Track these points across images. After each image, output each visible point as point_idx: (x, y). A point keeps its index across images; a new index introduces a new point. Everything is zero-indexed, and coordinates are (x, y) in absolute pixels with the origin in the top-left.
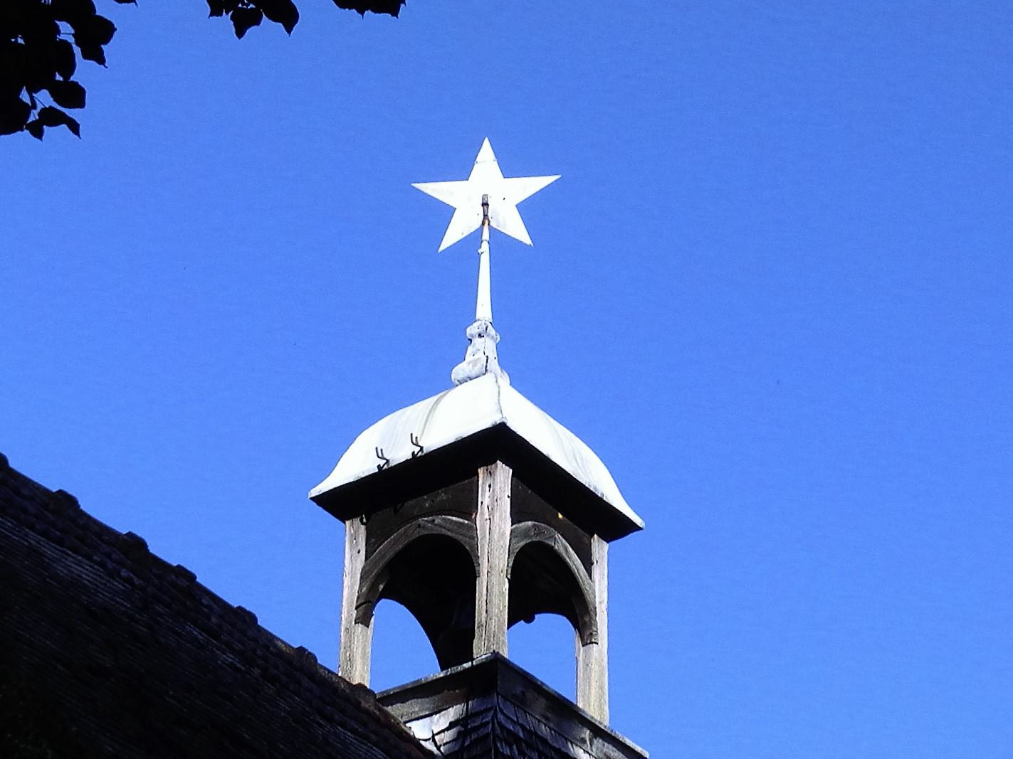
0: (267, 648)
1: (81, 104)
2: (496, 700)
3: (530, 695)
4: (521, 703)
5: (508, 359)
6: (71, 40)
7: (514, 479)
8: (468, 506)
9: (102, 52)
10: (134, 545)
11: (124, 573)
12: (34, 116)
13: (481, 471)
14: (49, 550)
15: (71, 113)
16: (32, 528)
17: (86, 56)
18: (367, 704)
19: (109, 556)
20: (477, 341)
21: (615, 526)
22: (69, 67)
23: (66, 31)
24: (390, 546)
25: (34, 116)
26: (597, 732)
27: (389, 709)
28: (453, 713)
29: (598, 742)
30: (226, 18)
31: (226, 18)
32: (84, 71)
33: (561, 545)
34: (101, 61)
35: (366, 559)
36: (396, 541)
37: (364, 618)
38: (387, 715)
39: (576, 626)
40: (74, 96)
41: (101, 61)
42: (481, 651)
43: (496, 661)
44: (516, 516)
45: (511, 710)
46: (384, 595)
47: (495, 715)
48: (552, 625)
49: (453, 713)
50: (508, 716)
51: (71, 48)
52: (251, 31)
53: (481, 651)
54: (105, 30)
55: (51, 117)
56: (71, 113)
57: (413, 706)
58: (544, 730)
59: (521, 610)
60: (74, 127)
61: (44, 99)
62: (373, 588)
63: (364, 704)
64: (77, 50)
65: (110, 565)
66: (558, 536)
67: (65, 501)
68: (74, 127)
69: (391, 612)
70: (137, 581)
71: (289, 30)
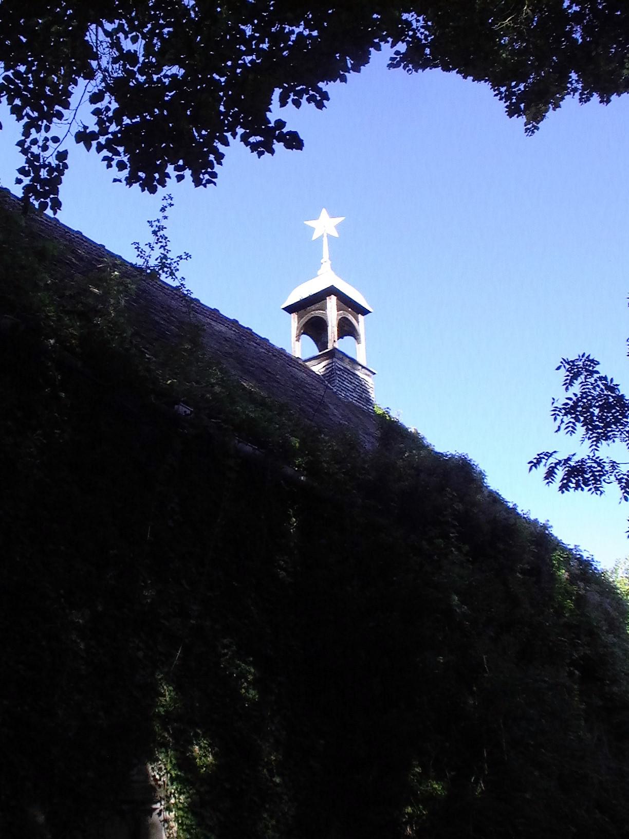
0: (273, 348)
1: (216, 178)
2: (335, 359)
3: (344, 358)
4: (342, 360)
5: (333, 268)
6: (213, 159)
7: (326, 340)
8: (324, 308)
9: (221, 162)
10: (235, 322)
11: (234, 329)
12: (204, 182)
13: (327, 298)
14: (213, 323)
15: (213, 180)
16: (208, 318)
17: (218, 164)
18: (300, 362)
19: (229, 324)
20: (324, 263)
21: (365, 312)
22: (212, 168)
23: (212, 157)
24: (305, 319)
25: (204, 182)
26: (363, 367)
27: (306, 363)
28: (324, 363)
29: (363, 369)
30: (255, 153)
31: (255, 153)
32: (217, 168)
33: (350, 317)
34: (221, 165)
35: (298, 323)
36: (306, 319)
37: (298, 339)
38: (306, 365)
39: (356, 339)
40: (214, 175)
41: (221, 165)
42: (330, 347)
43: (335, 350)
44: (338, 310)
45: (339, 362)
46: (303, 334)
47: (335, 364)
48: (349, 339)
49: (324, 363)
50: (339, 364)
51: (213, 162)
52: (262, 157)
53: (330, 347)
54: (222, 156)
55: (209, 182)
56: (213, 180)
57: (313, 362)
58: (349, 367)
59: (340, 336)
60: (215, 184)
61: (207, 177)
62: (300, 331)
63: (299, 362)
64: (215, 162)
65: (230, 327)
66: (349, 315)
67: (216, 310)
68: (215, 184)
69: (305, 338)
70: (237, 331)
71: (273, 155)
